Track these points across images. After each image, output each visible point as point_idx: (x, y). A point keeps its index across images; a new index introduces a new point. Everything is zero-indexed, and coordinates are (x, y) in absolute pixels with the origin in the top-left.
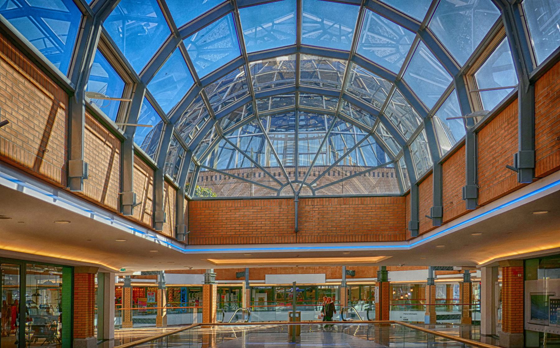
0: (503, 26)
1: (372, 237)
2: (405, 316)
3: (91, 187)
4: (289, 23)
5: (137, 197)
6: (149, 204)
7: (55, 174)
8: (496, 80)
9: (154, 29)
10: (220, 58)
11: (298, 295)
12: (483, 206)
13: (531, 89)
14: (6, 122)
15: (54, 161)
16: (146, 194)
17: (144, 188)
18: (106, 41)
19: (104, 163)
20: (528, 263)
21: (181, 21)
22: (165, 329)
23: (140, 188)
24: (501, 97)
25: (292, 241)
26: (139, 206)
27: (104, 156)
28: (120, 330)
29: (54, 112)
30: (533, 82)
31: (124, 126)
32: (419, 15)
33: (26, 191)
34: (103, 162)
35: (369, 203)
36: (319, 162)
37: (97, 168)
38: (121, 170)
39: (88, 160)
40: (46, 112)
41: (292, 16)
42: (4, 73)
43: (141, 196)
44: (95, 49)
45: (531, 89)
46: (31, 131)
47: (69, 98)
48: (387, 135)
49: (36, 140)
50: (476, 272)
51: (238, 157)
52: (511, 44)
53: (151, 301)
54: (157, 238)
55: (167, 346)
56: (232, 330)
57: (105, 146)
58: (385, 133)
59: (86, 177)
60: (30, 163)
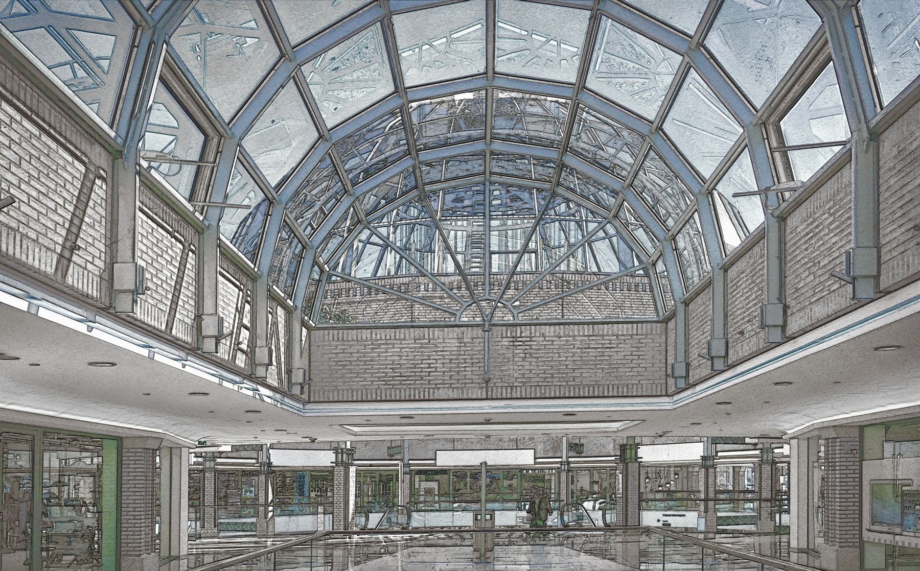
0: (826, 42)
1: (611, 389)
2: (665, 518)
3: (150, 306)
4: (475, 39)
5: (226, 324)
6: (245, 334)
7: (31, 258)
8: (815, 131)
9: (252, 49)
10: (361, 95)
11: (248, 296)
12: (795, 338)
13: (871, 149)
14: (12, 200)
15: (88, 264)
16: (241, 319)
17: (237, 308)
18: (174, 66)
19: (171, 268)
20: (868, 432)
21: (295, 33)
22: (272, 539)
23: (230, 308)
24: (824, 157)
25: (479, 397)
26: (229, 338)
27: (172, 257)
28: (198, 541)
29: (185, 257)
30: (875, 136)
31: (204, 206)
32: (689, 23)
33: (43, 313)
34: (159, 259)
35: (605, 333)
36: (524, 266)
37: (159, 275)
38: (288, 342)
39: (145, 263)
40: (75, 183)
41: (478, 29)
42: (7, 121)
43: (232, 322)
44: (156, 80)
45: (871, 149)
46: (50, 215)
47: (113, 162)
48: (830, 42)
49: (58, 230)
50: (782, 448)
51: (390, 259)
52: (840, 73)
53: (248, 494)
54: (258, 390)
55: (275, 570)
56: (382, 542)
57: (173, 240)
58: (633, 219)
59: (486, 463)
60: (46, 264)
